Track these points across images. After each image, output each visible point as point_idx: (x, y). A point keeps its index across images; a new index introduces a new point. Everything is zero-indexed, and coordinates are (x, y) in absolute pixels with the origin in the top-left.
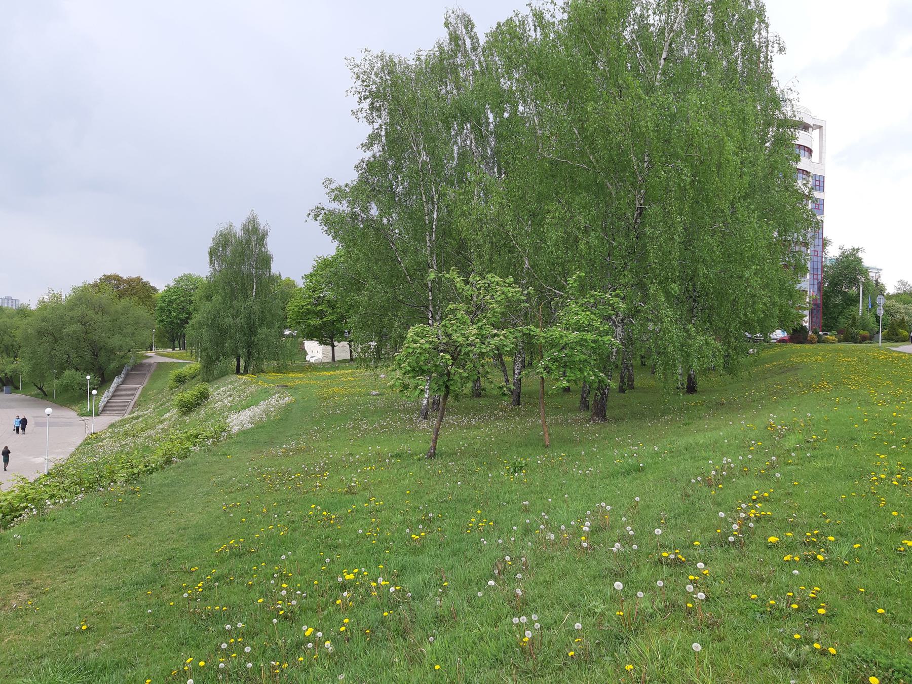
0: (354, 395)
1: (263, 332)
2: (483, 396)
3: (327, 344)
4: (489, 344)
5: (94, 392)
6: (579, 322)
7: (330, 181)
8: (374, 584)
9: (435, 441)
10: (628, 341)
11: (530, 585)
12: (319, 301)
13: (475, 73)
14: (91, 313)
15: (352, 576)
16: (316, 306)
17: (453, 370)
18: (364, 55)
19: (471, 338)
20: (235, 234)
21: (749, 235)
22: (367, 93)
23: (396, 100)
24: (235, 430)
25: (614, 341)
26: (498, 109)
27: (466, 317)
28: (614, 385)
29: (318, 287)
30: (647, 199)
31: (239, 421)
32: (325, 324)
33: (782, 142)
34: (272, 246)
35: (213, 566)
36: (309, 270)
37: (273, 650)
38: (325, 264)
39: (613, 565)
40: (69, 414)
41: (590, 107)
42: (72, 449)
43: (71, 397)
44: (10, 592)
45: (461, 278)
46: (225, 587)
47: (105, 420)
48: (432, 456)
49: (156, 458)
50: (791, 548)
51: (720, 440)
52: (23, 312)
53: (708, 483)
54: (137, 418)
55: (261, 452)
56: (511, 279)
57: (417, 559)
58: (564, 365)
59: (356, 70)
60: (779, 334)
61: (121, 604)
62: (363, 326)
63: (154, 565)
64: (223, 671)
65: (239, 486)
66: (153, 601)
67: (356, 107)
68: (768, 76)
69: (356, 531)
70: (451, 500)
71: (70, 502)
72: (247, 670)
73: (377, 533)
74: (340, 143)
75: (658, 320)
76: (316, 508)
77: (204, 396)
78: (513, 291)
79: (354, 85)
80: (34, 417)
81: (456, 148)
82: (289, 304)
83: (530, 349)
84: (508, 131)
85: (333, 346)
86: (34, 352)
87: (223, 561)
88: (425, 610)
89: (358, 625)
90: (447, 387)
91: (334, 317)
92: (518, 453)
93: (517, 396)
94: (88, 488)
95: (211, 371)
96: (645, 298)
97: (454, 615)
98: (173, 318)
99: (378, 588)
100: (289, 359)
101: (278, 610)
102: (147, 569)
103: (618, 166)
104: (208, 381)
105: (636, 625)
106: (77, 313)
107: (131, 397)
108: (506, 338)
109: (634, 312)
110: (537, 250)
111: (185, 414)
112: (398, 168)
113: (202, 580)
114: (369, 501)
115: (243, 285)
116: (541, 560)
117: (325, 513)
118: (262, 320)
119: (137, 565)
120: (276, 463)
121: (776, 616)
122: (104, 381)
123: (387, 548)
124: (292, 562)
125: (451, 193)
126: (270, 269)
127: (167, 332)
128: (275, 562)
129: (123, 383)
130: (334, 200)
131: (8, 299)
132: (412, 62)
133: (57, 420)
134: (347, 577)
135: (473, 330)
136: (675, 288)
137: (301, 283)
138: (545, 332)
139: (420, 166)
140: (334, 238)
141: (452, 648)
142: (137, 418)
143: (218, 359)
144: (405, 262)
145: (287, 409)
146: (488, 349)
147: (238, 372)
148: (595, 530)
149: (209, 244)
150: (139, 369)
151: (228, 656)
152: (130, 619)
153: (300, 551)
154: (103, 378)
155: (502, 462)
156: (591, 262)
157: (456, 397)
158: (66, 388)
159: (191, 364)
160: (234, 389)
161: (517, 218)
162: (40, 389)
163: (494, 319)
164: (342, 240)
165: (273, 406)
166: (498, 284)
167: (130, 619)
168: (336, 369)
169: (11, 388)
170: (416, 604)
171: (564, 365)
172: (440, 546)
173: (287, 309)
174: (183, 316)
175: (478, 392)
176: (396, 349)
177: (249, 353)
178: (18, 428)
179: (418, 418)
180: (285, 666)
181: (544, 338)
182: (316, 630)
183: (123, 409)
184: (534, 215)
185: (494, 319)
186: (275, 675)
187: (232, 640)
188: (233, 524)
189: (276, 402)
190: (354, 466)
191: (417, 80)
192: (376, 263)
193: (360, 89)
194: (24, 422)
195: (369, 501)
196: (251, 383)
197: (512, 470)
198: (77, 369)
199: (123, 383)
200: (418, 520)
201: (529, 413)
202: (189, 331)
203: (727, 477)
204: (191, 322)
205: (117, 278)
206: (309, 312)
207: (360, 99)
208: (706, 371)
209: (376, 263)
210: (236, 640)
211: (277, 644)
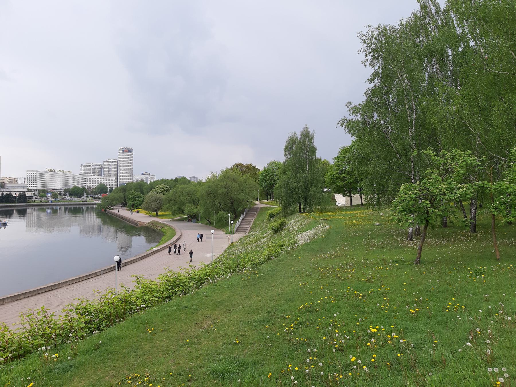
0: (365, 225)
1: (312, 190)
2: (450, 227)
3: (347, 196)
4: (456, 193)
5: (232, 222)
7: (350, 103)
8: (389, 336)
9: (420, 254)
11: (496, 348)
13: (438, 27)
14: (230, 183)
15: (375, 330)
16: (341, 174)
17: (431, 210)
18: (368, 29)
19: (443, 190)
20: (297, 138)
22: (370, 50)
23: (388, 51)
24: (301, 243)
26: (454, 47)
27: (439, 177)
29: (342, 164)
31: (303, 238)
32: (346, 184)
34: (317, 143)
35: (298, 316)
36: (337, 155)
37: (334, 367)
38: (345, 151)
40: (221, 233)
42: (223, 250)
43: (222, 224)
44: (203, 320)
45: (435, 153)
46: (304, 329)
48: (418, 263)
49: (263, 256)
52: (200, 183)
54: (252, 235)
55: (316, 255)
56: (469, 151)
57: (414, 324)
59: (363, 38)
61: (253, 332)
63: (268, 312)
64: (308, 374)
65: (306, 274)
66: (269, 331)
67: (364, 59)
69: (375, 304)
70: (434, 290)
71: (226, 277)
72: (321, 376)
73: (388, 306)
74: (353, 79)
76: (350, 289)
78: (472, 159)
79: (362, 47)
80: (206, 234)
81: (426, 74)
82: (326, 174)
84: (460, 60)
85: (351, 197)
86: (205, 203)
87: (302, 314)
89: (382, 359)
90: (427, 221)
91: (351, 180)
92: (477, 264)
94: (233, 270)
95: (287, 211)
98: (267, 183)
99: (392, 339)
101: (334, 345)
102: (265, 314)
104: (285, 216)
106: (223, 183)
107: (249, 225)
108: (468, 190)
110: (487, 132)
111: (274, 234)
113: (293, 323)
114: (381, 287)
115: (301, 165)
117: (355, 292)
118: (312, 184)
119: (260, 312)
120: (325, 262)
122: (236, 217)
123: (395, 316)
124: (340, 318)
126: (316, 155)
127: (265, 191)
128: (330, 317)
129: (245, 217)
130: (352, 114)
131: (193, 177)
132: (397, 27)
133: (216, 236)
134: (373, 330)
135: (444, 185)
137: (332, 162)
138: (495, 185)
139: (404, 87)
140: (353, 135)
141: (444, 381)
142: (252, 235)
143: (290, 205)
144: (395, 146)
145: (328, 232)
146: (455, 197)
147: (300, 212)
149: (284, 144)
150: (252, 210)
151: (309, 366)
152: (259, 340)
153: (343, 313)
154: (236, 215)
155: (467, 269)
157: (433, 227)
158: (220, 220)
159: (276, 208)
160: (299, 221)
161: (472, 114)
162: (208, 220)
163: (458, 178)
164: (358, 136)
165: (320, 231)
166: (460, 155)
167: (259, 340)
168: (352, 210)
169: (195, 220)
170: (417, 351)
172: (429, 318)
173: (325, 177)
174: (272, 183)
175: (445, 225)
177: (305, 201)
178: (198, 239)
179: (407, 239)
180: (341, 376)
181: (494, 189)
182: (357, 359)
183: (245, 231)
184: (482, 110)
185: (458, 178)
186: (336, 381)
187: (311, 358)
188: (306, 295)
189: (321, 228)
191: (401, 37)
192: (377, 148)
193: (366, 48)
194: (202, 236)
195: (381, 287)
196: (308, 218)
197: (474, 274)
198: (224, 211)
199: (245, 217)
200: (413, 301)
202: (275, 190)
204: (276, 186)
205: (241, 165)
206: (337, 178)
207: (366, 54)
209: (377, 148)
210: (313, 358)
211: (335, 363)
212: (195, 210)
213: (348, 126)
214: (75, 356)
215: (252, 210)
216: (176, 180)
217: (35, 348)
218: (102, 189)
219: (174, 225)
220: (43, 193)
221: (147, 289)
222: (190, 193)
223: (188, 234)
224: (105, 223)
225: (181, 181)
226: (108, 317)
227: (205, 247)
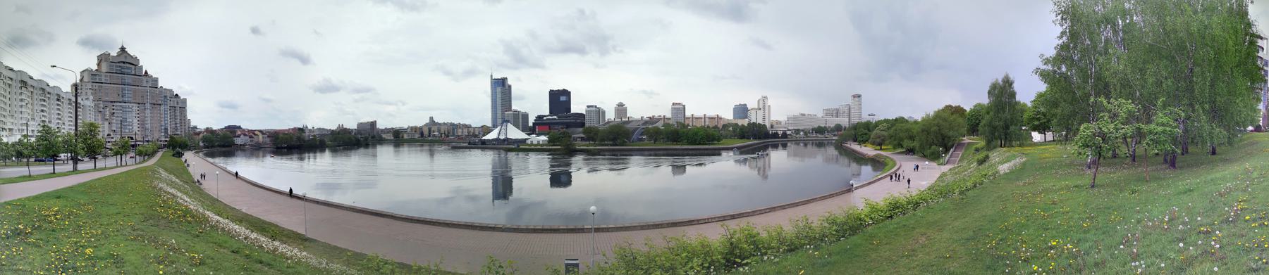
1: (1012, 128)
6: (1163, 122)
10: (1186, 131)
12: (1038, 113)
21: (1238, 84)
23: (1074, 14)
25: (1179, 131)
26: (1124, 18)
28: (1179, 152)
30: (1195, 64)
31: (1004, 168)
33: (1252, 43)
34: (1016, 87)
38: (1041, 95)
39: (1179, 236)
40: (934, 164)
41: (1168, 19)
43: (935, 157)
47: (948, 167)
49: (970, 184)
50: (1254, 221)
51: (1226, 176)
52: (916, 122)
53: (1221, 195)
58: (1156, 142)
60: (1250, 128)
62: (1059, 124)
68: (1247, 13)
75: (1199, 121)
77: (987, 157)
83: (1140, 135)
84: (1128, 29)
88: (1090, 260)
93: (1134, 158)
95: (990, 146)
96: (1193, 111)
97: (1104, 262)
98: (973, 122)
100: (1025, 141)
102: (971, 233)
103: (1181, 48)
105: (1189, 262)
108: (1128, 130)
109: (1188, 118)
112: (1075, 47)
116: (1145, 235)
121: (1248, 251)
122: (947, 151)
125: (1101, 60)
135: (1112, 126)
136: (1207, 106)
137: (1029, 105)
144: (1079, 93)
145: (1024, 164)
148: (1170, 220)
150: (960, 145)
156: (1168, 93)
158: (933, 154)
159: (980, 142)
171: (1156, 142)
175: (1115, 156)
176: (1075, 135)
184: (1141, 70)
189: (1019, 161)
190: (1056, 191)
201: (1139, 165)
202: (980, 128)
203: (1229, 192)
208: (1220, 145)
212: (911, 144)
213: (1041, 75)
214: (830, 255)
215: (960, 145)
216: (896, 120)
217: (802, 246)
218: (838, 128)
219: (895, 157)
220: (797, 132)
221: (874, 209)
222: (907, 130)
223: (906, 165)
224: (841, 154)
225: (901, 120)
226: (850, 228)
227: (921, 176)
